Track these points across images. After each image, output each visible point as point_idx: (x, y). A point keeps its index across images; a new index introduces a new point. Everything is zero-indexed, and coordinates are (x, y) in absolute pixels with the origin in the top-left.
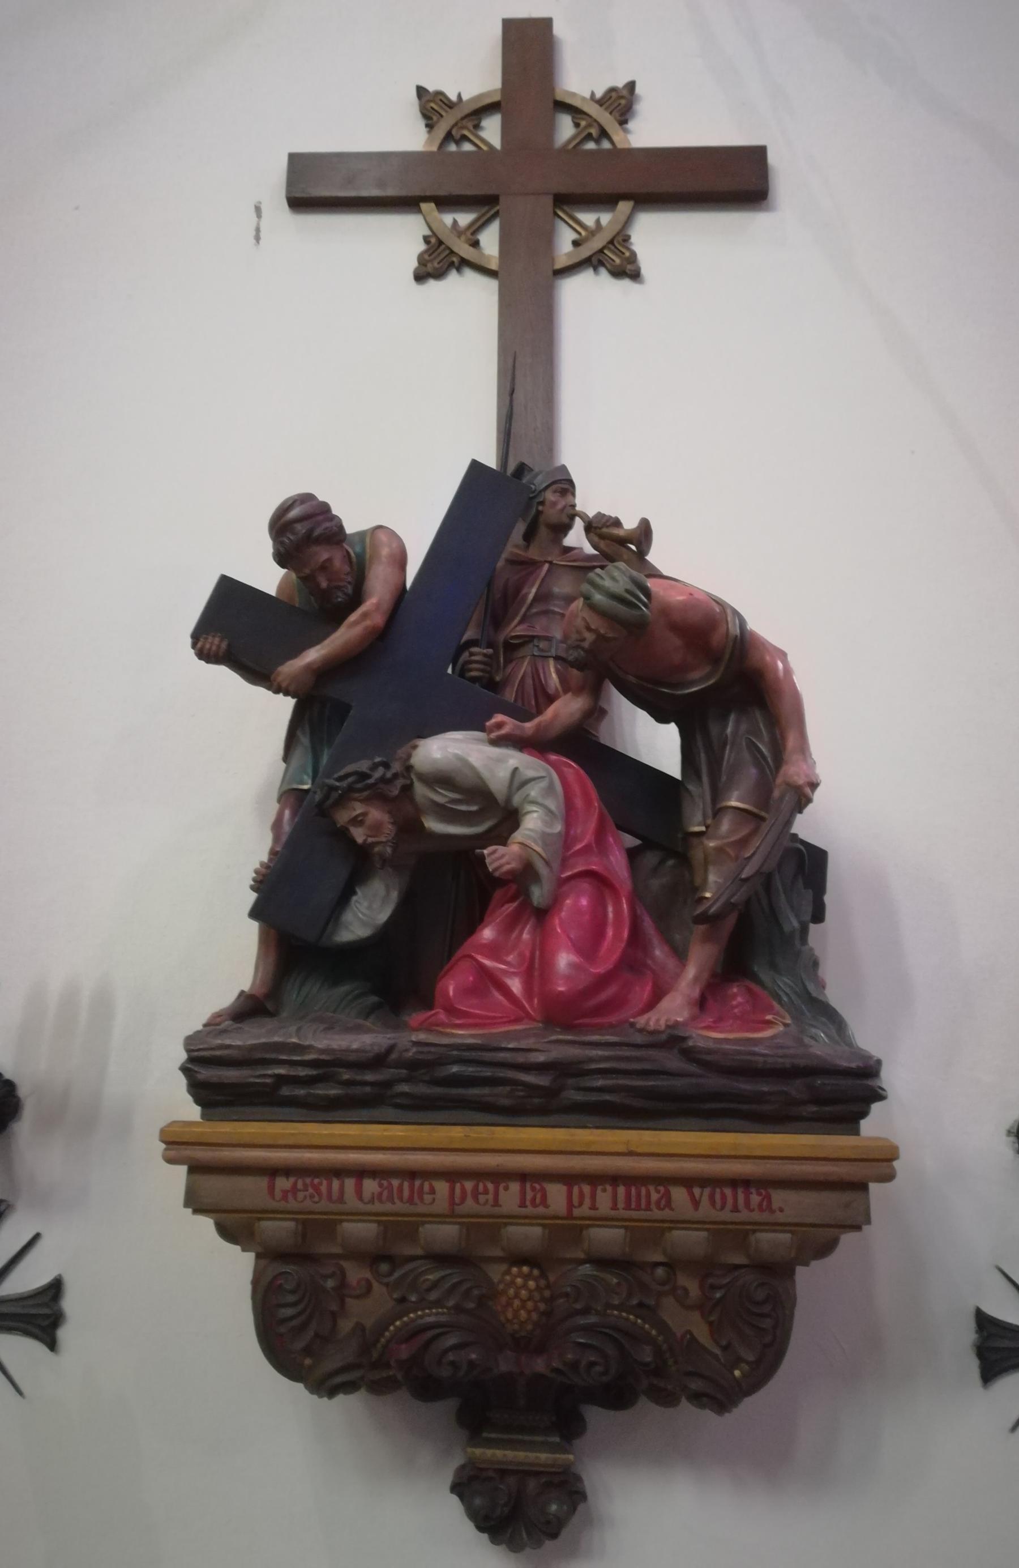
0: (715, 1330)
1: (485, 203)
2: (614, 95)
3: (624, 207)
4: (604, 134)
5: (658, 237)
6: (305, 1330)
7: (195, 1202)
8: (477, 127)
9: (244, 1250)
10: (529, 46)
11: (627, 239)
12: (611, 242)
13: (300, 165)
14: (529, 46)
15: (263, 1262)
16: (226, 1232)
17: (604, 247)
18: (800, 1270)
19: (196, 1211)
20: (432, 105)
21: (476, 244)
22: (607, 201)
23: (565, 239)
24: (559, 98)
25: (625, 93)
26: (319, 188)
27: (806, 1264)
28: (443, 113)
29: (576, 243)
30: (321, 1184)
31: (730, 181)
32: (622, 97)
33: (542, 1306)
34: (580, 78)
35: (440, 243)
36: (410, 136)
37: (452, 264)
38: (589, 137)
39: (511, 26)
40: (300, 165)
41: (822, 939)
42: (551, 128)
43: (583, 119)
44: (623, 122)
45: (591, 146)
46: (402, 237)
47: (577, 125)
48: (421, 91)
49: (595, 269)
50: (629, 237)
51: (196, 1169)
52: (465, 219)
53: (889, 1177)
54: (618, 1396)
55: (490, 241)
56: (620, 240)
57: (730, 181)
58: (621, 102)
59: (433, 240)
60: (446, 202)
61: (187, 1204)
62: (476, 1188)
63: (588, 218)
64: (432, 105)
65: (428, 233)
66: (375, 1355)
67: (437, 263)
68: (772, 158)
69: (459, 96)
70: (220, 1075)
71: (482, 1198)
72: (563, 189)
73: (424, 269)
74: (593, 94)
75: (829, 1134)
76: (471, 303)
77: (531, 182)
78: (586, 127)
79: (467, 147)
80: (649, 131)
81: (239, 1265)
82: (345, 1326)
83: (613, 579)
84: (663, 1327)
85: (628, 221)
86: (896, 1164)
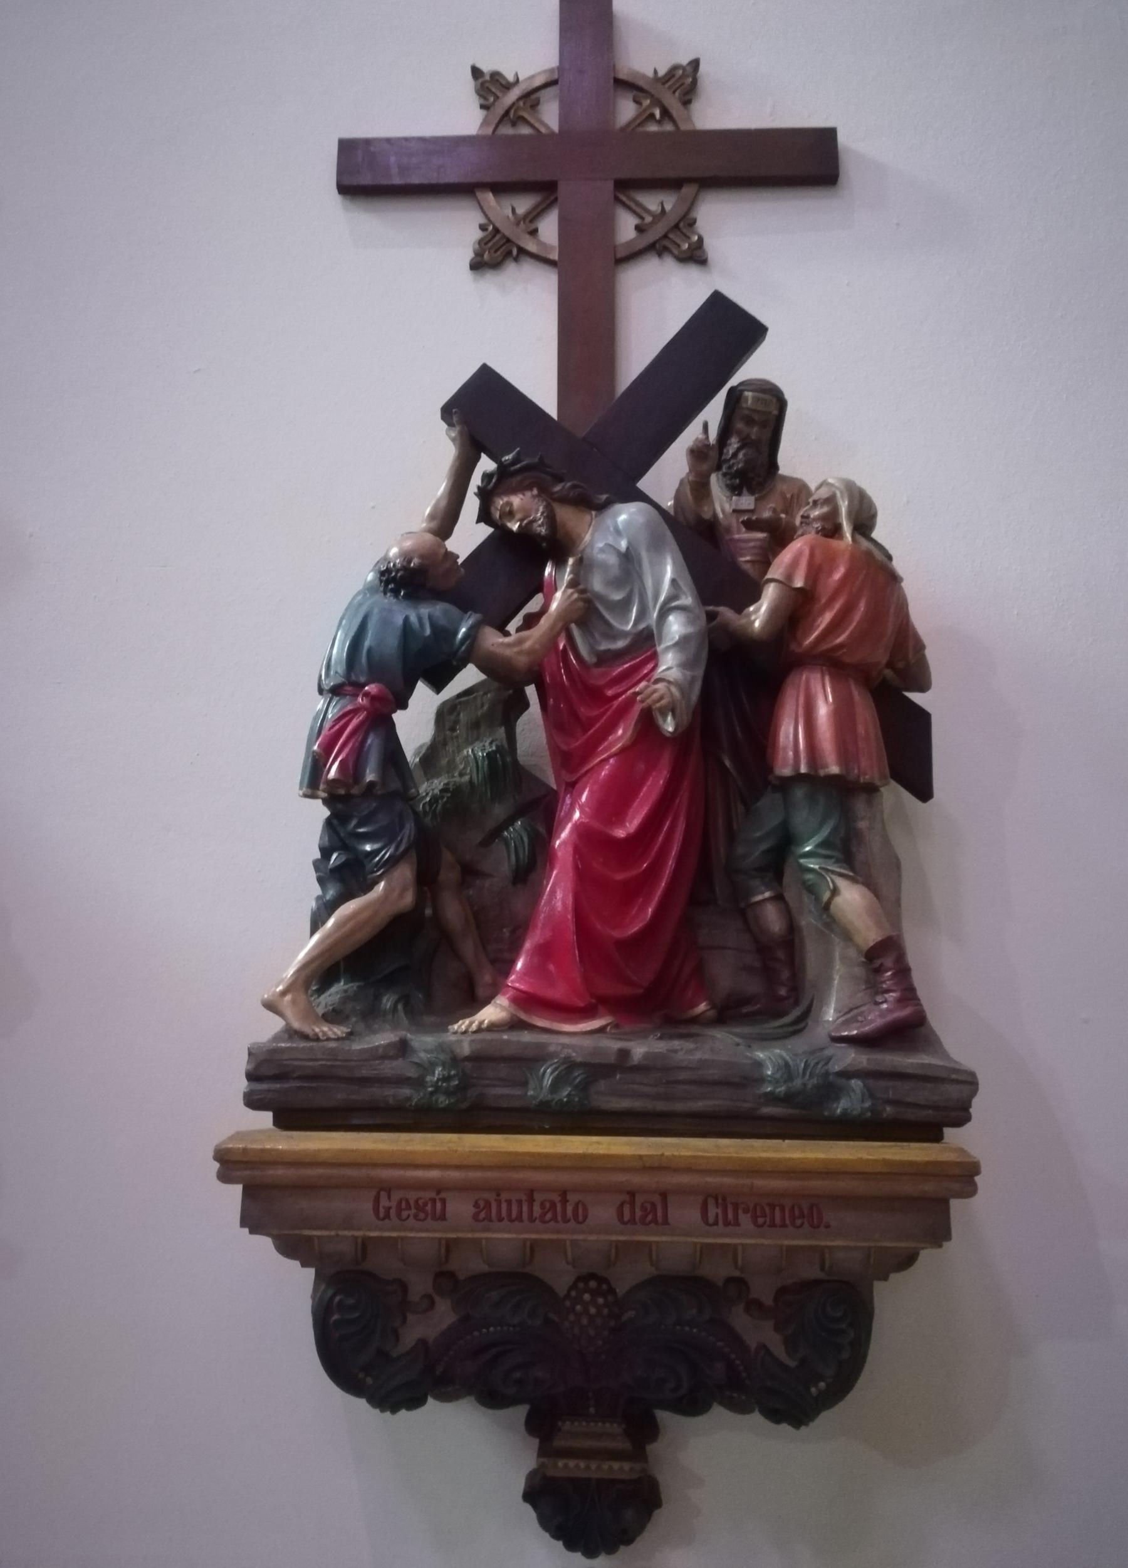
0: (791, 1344)
1: (546, 191)
3: (688, 190)
4: (666, 113)
6: (371, 1343)
9: (303, 1265)
11: (692, 223)
13: (351, 152)
15: (481, 992)
18: (878, 1286)
20: (489, 85)
21: (534, 232)
22: (674, 184)
23: (626, 227)
24: (622, 76)
26: (372, 177)
28: (499, 94)
29: (639, 228)
35: (496, 231)
36: (465, 118)
37: (509, 253)
40: (351, 152)
42: (610, 110)
43: (646, 98)
44: (687, 103)
45: (653, 128)
46: (458, 229)
47: (637, 102)
49: (660, 255)
50: (695, 221)
51: (249, 1193)
52: (523, 204)
55: (549, 229)
56: (685, 223)
60: (500, 189)
61: (244, 1223)
63: (652, 202)
64: (489, 85)
65: (483, 221)
66: (439, 1370)
67: (495, 254)
70: (285, 1085)
71: (405, 1214)
72: (624, 174)
73: (479, 259)
75: (848, 1392)
78: (649, 107)
81: (299, 1281)
84: (736, 1339)
85: (692, 205)
86: (977, 1179)
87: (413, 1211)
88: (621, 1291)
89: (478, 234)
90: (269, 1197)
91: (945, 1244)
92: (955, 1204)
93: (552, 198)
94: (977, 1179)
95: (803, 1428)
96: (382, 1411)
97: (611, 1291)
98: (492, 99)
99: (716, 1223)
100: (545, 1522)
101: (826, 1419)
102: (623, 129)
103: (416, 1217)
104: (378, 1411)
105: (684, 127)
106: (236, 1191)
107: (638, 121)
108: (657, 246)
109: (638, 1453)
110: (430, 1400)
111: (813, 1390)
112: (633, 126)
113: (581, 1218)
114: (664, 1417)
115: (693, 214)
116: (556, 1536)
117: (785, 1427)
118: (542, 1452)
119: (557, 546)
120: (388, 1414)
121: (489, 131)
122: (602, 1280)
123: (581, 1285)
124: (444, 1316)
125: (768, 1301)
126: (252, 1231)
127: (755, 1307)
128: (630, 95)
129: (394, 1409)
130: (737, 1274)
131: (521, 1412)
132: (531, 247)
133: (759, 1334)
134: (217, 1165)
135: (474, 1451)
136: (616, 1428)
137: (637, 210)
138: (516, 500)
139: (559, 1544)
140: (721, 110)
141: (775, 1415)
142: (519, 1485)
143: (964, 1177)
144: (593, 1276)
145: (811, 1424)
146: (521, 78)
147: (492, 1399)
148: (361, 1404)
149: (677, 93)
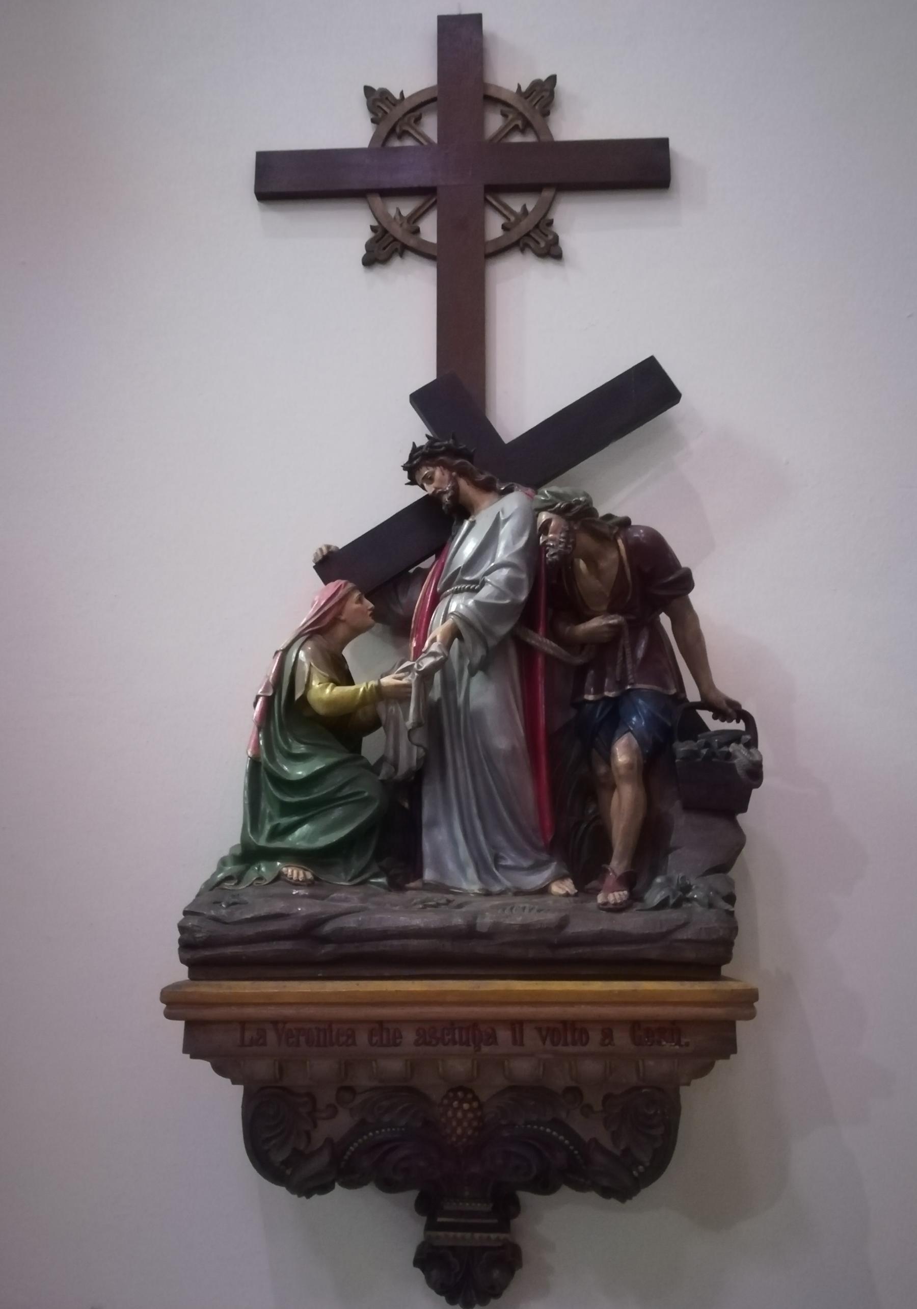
2: (538, 88)
3: (547, 194)
5: (581, 222)
6: (293, 1141)
7: (193, 1048)
8: (418, 120)
9: (234, 1083)
10: (460, 38)
11: (550, 223)
12: (537, 226)
13: (266, 164)
14: (460, 38)
16: (220, 1070)
18: (683, 1090)
20: (378, 101)
21: (417, 231)
22: (534, 188)
23: (494, 227)
26: (290, 181)
29: (504, 228)
31: (639, 169)
33: (475, 1124)
34: (509, 74)
35: (385, 232)
36: (354, 131)
38: (516, 128)
39: (443, 21)
40: (266, 164)
41: (720, 1063)
44: (546, 113)
45: (517, 139)
46: (352, 227)
47: (505, 115)
48: (368, 90)
51: (191, 1026)
52: (407, 207)
55: (429, 229)
56: (544, 225)
57: (639, 169)
59: (380, 230)
61: (185, 1051)
63: (516, 203)
64: (378, 101)
65: (375, 223)
67: (382, 250)
69: (402, 93)
76: (414, 288)
77: (468, 173)
78: (512, 120)
79: (409, 142)
81: (231, 1095)
82: (319, 1138)
83: (552, 555)
85: (549, 206)
86: (755, 1004)
88: (484, 1096)
89: (368, 235)
90: (207, 1034)
91: (732, 1056)
92: (740, 1025)
93: (434, 200)
95: (628, 1202)
96: (299, 1196)
97: (475, 1098)
98: (380, 115)
100: (430, 1282)
101: (646, 1193)
102: (491, 140)
104: (296, 1196)
105: (544, 138)
106: (179, 1026)
107: (503, 134)
108: (398, 130)
109: (504, 1225)
110: (337, 1186)
111: (635, 1173)
112: (500, 137)
114: (526, 1197)
115: (550, 217)
116: (440, 1293)
117: (613, 1202)
118: (429, 1227)
119: (462, 511)
120: (304, 1198)
122: (466, 1090)
123: (451, 1094)
124: (344, 1122)
126: (193, 1057)
127: (587, 1110)
128: (500, 108)
129: (308, 1194)
130: (573, 1084)
131: (412, 1196)
132: (411, 242)
133: (590, 1129)
135: (374, 1228)
136: (486, 1207)
137: (503, 210)
138: (438, 473)
139: (443, 1299)
140: (574, 124)
141: (606, 1193)
142: (410, 1253)
143: (746, 1001)
144: (461, 1088)
145: (634, 1198)
146: (406, 95)
147: (388, 1186)
148: (281, 1191)
149: (537, 107)
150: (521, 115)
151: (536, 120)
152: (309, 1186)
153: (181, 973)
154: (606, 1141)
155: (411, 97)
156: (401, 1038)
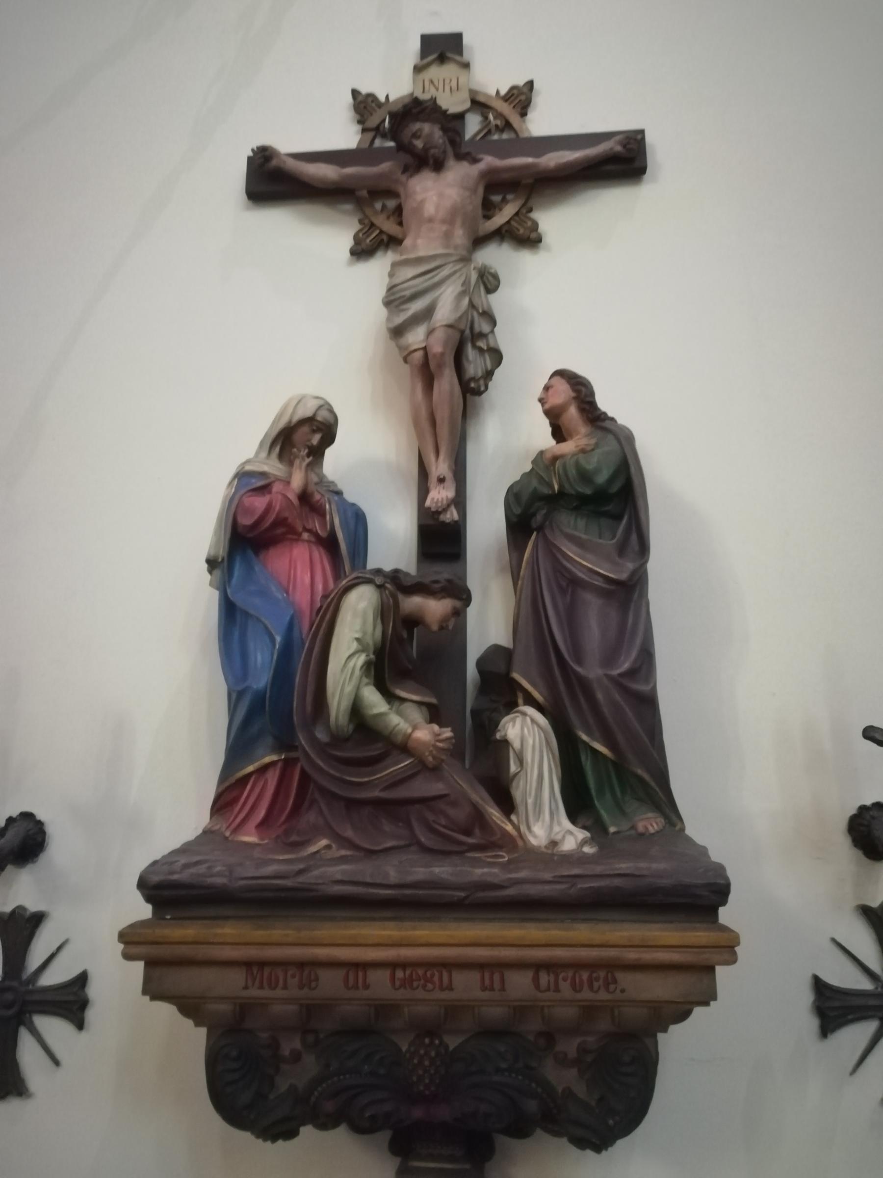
7: (153, 990)
17: (510, 219)
18: (661, 1036)
19: (154, 998)
20: (363, 105)
25: (525, 90)
26: (272, 181)
27: (665, 1030)
30: (433, 976)
31: (620, 161)
32: (522, 94)
36: (345, 136)
44: (523, 114)
45: (496, 137)
48: (355, 93)
51: (151, 964)
53: (732, 959)
54: (520, 1129)
57: (620, 161)
58: (521, 98)
61: (145, 992)
62: (590, 977)
68: (649, 138)
69: (387, 97)
74: (498, 92)
77: (440, 172)
80: (541, 122)
86: (737, 949)
87: (422, 982)
92: (721, 971)
94: (737, 949)
95: (604, 1152)
99: (548, 990)
103: (424, 987)
106: (139, 967)
113: (578, 988)
121: (366, 145)
124: (311, 1066)
125: (572, 1053)
127: (563, 1061)
129: (274, 1138)
131: (385, 1136)
133: (563, 1078)
134: (121, 946)
143: (728, 948)
145: (610, 1149)
146: (391, 99)
147: (362, 1128)
150: (499, 115)
151: (514, 119)
152: (279, 1130)
153: (145, 911)
154: (580, 1090)
155: (396, 101)
156: (317, 979)
